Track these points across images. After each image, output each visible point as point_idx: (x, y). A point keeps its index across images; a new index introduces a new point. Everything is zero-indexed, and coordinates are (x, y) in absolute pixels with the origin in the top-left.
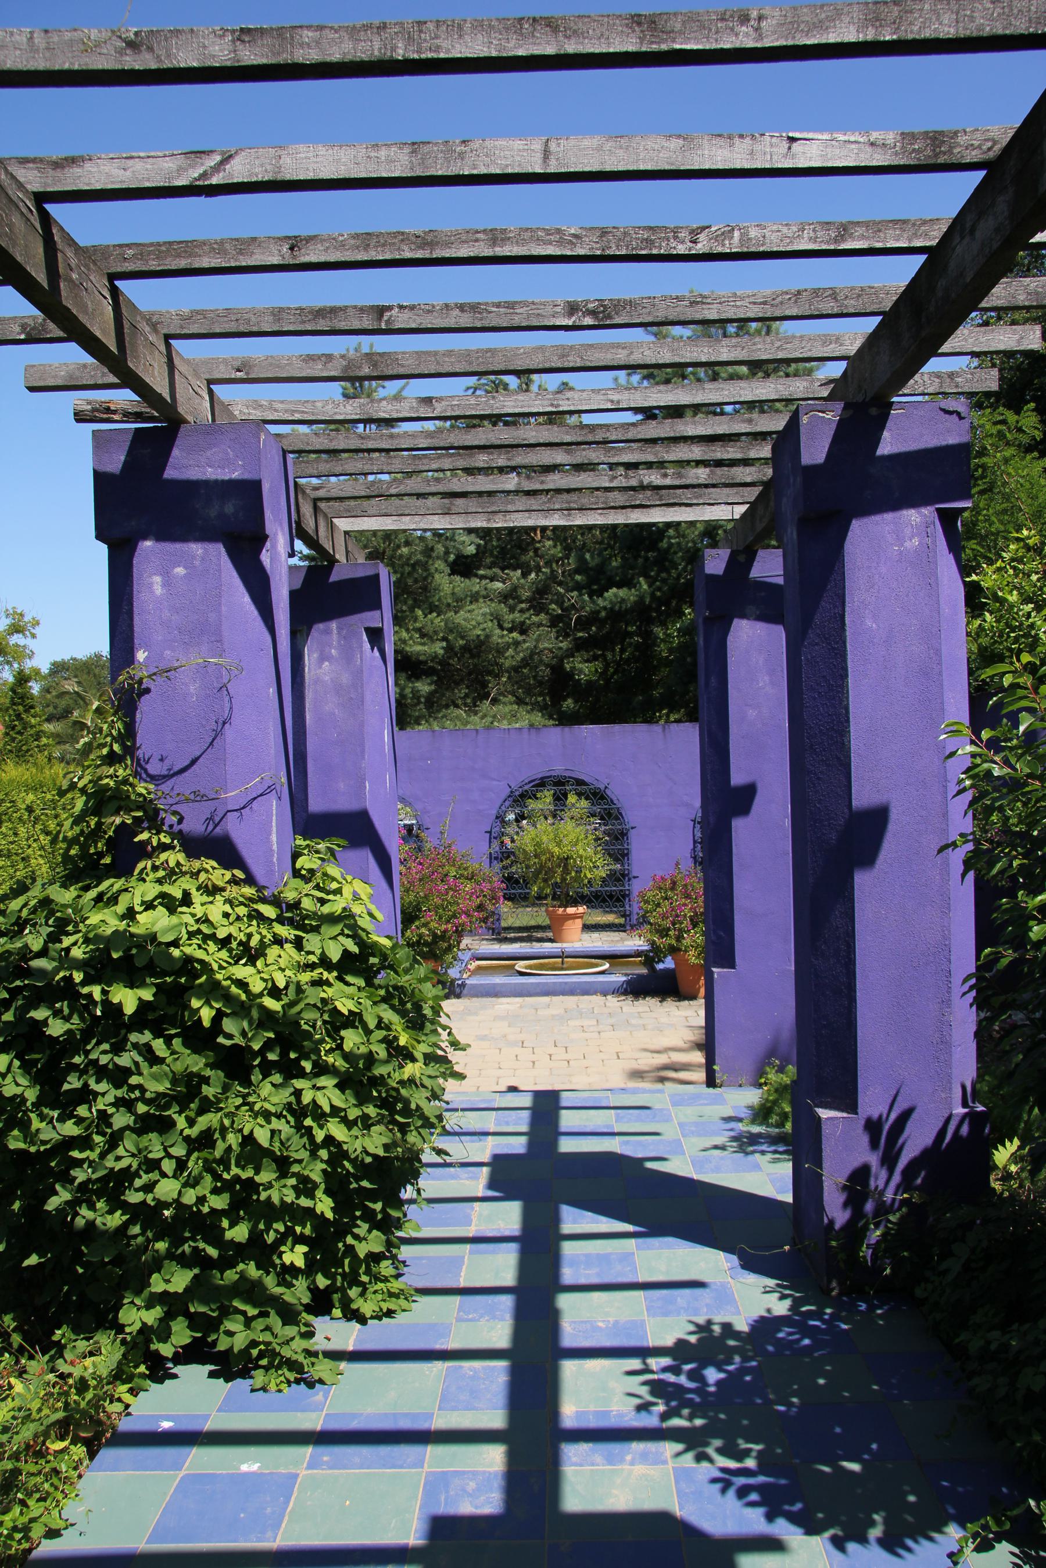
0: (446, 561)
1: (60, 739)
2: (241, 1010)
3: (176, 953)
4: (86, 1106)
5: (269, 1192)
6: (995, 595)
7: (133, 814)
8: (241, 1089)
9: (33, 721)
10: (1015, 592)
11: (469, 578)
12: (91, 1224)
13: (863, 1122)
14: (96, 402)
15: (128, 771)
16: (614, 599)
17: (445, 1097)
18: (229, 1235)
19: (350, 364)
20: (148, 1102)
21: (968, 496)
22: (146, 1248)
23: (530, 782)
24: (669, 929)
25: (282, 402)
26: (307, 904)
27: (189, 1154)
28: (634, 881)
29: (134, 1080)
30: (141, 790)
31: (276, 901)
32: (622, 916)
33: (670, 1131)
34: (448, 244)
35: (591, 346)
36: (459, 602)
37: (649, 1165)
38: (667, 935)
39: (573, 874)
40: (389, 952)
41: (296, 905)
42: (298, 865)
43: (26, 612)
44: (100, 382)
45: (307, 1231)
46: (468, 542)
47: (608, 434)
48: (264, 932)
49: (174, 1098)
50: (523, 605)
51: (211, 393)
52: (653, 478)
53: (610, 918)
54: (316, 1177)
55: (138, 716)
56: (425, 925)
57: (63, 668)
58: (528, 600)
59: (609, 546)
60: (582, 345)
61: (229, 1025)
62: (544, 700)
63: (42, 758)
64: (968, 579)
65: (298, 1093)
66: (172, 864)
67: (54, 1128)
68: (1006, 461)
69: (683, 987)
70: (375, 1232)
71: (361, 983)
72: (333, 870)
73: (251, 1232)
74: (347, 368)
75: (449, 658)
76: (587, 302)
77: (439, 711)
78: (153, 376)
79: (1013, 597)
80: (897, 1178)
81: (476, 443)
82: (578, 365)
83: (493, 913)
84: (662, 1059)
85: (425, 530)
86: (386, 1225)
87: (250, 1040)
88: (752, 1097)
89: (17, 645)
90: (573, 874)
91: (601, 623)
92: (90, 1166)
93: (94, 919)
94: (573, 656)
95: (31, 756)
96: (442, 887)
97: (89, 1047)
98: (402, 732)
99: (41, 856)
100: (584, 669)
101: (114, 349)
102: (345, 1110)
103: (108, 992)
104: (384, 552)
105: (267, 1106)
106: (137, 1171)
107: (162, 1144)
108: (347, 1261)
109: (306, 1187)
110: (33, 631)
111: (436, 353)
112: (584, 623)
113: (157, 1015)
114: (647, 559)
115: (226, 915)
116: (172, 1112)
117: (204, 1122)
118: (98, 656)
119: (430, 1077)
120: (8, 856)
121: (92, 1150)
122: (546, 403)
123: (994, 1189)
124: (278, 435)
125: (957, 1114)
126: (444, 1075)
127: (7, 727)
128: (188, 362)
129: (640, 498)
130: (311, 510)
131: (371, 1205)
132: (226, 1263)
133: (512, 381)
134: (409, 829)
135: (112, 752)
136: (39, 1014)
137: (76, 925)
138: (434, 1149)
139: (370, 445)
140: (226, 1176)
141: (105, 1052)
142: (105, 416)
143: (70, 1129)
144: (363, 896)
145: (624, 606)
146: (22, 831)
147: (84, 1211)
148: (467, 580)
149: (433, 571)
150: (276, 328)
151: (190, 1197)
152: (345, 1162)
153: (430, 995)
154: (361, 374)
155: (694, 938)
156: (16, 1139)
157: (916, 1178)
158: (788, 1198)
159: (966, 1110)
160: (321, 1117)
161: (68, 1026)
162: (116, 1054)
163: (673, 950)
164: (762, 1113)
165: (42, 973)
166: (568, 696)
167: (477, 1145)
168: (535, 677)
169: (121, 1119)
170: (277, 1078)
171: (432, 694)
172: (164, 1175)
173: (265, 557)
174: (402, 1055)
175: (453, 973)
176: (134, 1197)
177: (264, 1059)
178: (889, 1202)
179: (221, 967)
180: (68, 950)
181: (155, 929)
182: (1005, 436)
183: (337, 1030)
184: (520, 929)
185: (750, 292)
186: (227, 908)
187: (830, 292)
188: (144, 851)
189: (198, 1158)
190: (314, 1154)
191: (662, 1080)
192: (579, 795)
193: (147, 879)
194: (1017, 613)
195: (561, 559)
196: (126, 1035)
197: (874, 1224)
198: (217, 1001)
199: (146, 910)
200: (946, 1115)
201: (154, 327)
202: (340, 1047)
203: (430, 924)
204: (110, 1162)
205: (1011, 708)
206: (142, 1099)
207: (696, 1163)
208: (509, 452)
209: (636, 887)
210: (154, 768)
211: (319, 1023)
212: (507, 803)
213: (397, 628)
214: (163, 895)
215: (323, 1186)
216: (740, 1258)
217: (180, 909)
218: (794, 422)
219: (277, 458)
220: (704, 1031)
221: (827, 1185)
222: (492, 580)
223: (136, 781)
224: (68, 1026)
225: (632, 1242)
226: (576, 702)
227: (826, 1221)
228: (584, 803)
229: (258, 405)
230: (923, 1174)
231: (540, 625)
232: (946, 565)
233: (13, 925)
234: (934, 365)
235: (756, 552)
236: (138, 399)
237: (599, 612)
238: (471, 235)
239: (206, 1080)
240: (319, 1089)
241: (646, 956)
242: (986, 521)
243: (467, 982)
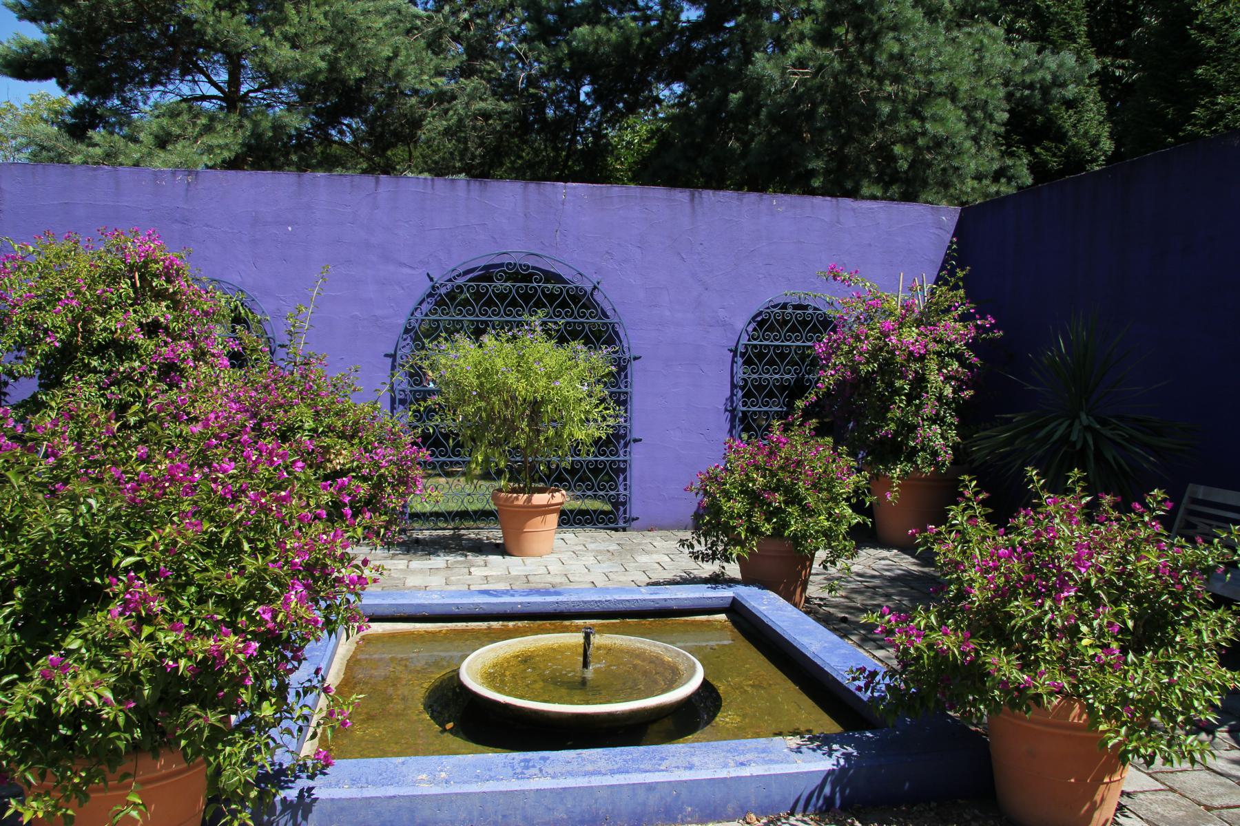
28: (634, 446)
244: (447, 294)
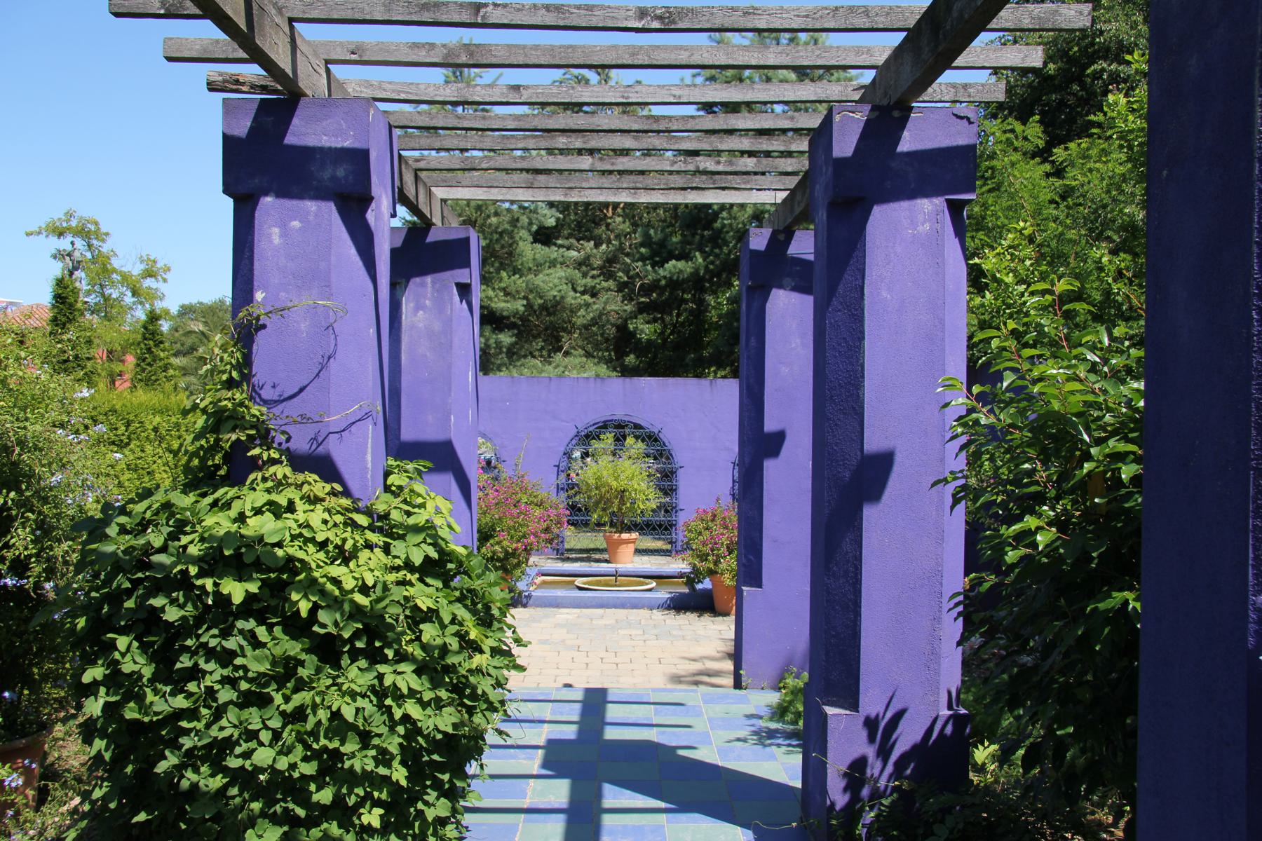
0: (529, 231)
1: (185, 372)
2: (335, 604)
3: (280, 552)
4: (195, 683)
5: (352, 761)
6: (994, 277)
7: (247, 432)
8: (332, 672)
9: (162, 355)
10: (1011, 275)
11: (549, 246)
12: (195, 786)
13: (863, 719)
14: (227, 74)
15: (244, 395)
16: (673, 270)
17: (508, 686)
18: (315, 798)
19: (451, 52)
20: (250, 681)
21: (972, 189)
22: (242, 808)
23: (594, 424)
24: (708, 555)
25: (390, 83)
26: (396, 516)
27: (284, 727)
28: (680, 513)
29: (239, 661)
30: (255, 411)
31: (368, 512)
32: (670, 543)
33: (700, 725)
35: (658, 47)
36: (538, 267)
37: (681, 752)
38: (706, 560)
39: (628, 505)
40: (464, 559)
41: (386, 516)
42: (389, 482)
43: (159, 259)
44: (230, 56)
45: (384, 796)
46: (549, 216)
47: (670, 124)
48: (357, 537)
49: (272, 677)
50: (595, 272)
51: (328, 71)
52: (708, 164)
53: (659, 544)
54: (394, 749)
55: (255, 347)
56: (499, 543)
57: (191, 310)
58: (601, 268)
59: (671, 225)
60: (650, 46)
61: (323, 616)
62: (610, 355)
63: (168, 387)
64: (971, 262)
65: (380, 677)
66: (280, 476)
67: (166, 701)
68: (1013, 164)
69: (718, 605)
70: (442, 799)
71: (439, 584)
72: (419, 487)
73: (335, 796)
74: (447, 56)
75: (529, 315)
76: (655, 8)
77: (518, 360)
78: (278, 53)
79: (1009, 279)
80: (890, 768)
81: (557, 127)
82: (646, 63)
83: (558, 536)
84: (697, 666)
85: (512, 202)
86: (453, 794)
87: (341, 629)
88: (774, 698)
89: (150, 288)
90: (628, 505)
91: (663, 289)
92: (196, 735)
93: (209, 521)
94: (636, 318)
95: (160, 384)
96: (515, 512)
97: (200, 632)
98: (486, 377)
99: (165, 471)
100: (645, 329)
101: (243, 27)
102: (420, 692)
103: (219, 584)
104: (476, 221)
105: (353, 686)
106: (238, 740)
107: (261, 717)
108: (417, 824)
109: (384, 758)
110: (164, 276)
111: (524, 47)
112: (646, 290)
113: (261, 605)
114: (702, 236)
115: (325, 522)
116: (270, 689)
117: (298, 699)
118: (222, 302)
119: (495, 667)
120: (136, 470)
121: (199, 721)
122: (618, 94)
123: (972, 781)
124: (385, 112)
125: (943, 716)
126: (507, 667)
127: (138, 359)
128: (309, 43)
129: (697, 181)
130: (413, 179)
131: (439, 775)
132: (311, 822)
133: (590, 75)
134: (489, 462)
135: (231, 379)
136: (158, 602)
137: (194, 526)
138: (497, 730)
139: (466, 124)
140: (315, 746)
141: (214, 636)
142: (234, 87)
143: (180, 702)
144: (444, 511)
145: (681, 277)
146: (149, 448)
147: (189, 774)
148: (547, 249)
149: (517, 239)
150: (386, 18)
151: (283, 764)
152: (419, 738)
153: (498, 598)
154: (459, 61)
155: (729, 563)
156: (132, 710)
157: (907, 769)
158: (798, 784)
159: (951, 712)
160: (399, 697)
161: (182, 613)
162: (224, 639)
163: (711, 573)
164: (780, 712)
165: (161, 566)
166: (630, 352)
167: (535, 731)
168: (602, 335)
169: (225, 695)
170: (363, 663)
171: (513, 345)
172: (261, 744)
173: (370, 216)
174: (472, 648)
175: (521, 586)
176: (233, 763)
177: (353, 646)
178: (882, 788)
179: (319, 566)
180: (185, 547)
181: (262, 531)
182: (1012, 144)
183: (417, 624)
184: (581, 551)
185: (794, 6)
186: (326, 516)
187: (864, 9)
188: (255, 464)
189: (292, 730)
190: (392, 729)
191: (697, 683)
192: (637, 437)
193: (258, 488)
194: (1011, 293)
195: (629, 233)
196: (233, 622)
197: (869, 807)
198: (314, 595)
199: (255, 515)
200: (934, 716)
201: (280, 10)
202: (418, 639)
203: (503, 543)
204: (214, 732)
205: (997, 368)
206: (245, 678)
207: (722, 752)
208: (584, 136)
209: (681, 518)
210: (267, 394)
211: (402, 617)
212: (574, 442)
213: (484, 287)
214: (271, 503)
215: (399, 758)
216: (755, 833)
217: (284, 515)
218: (828, 121)
219: (383, 131)
220: (733, 643)
221: (831, 773)
222: (568, 249)
223: (251, 404)
224: (182, 613)
225: (664, 816)
226: (637, 357)
227: (828, 802)
228: (640, 445)
229: (368, 84)
230: (912, 766)
231: (609, 289)
232: (952, 245)
233: (137, 525)
234: (948, 76)
235: (794, 232)
236: (265, 74)
237: (660, 280)
239: (302, 663)
240: (399, 673)
241: (688, 577)
242: (993, 215)
243: (533, 594)
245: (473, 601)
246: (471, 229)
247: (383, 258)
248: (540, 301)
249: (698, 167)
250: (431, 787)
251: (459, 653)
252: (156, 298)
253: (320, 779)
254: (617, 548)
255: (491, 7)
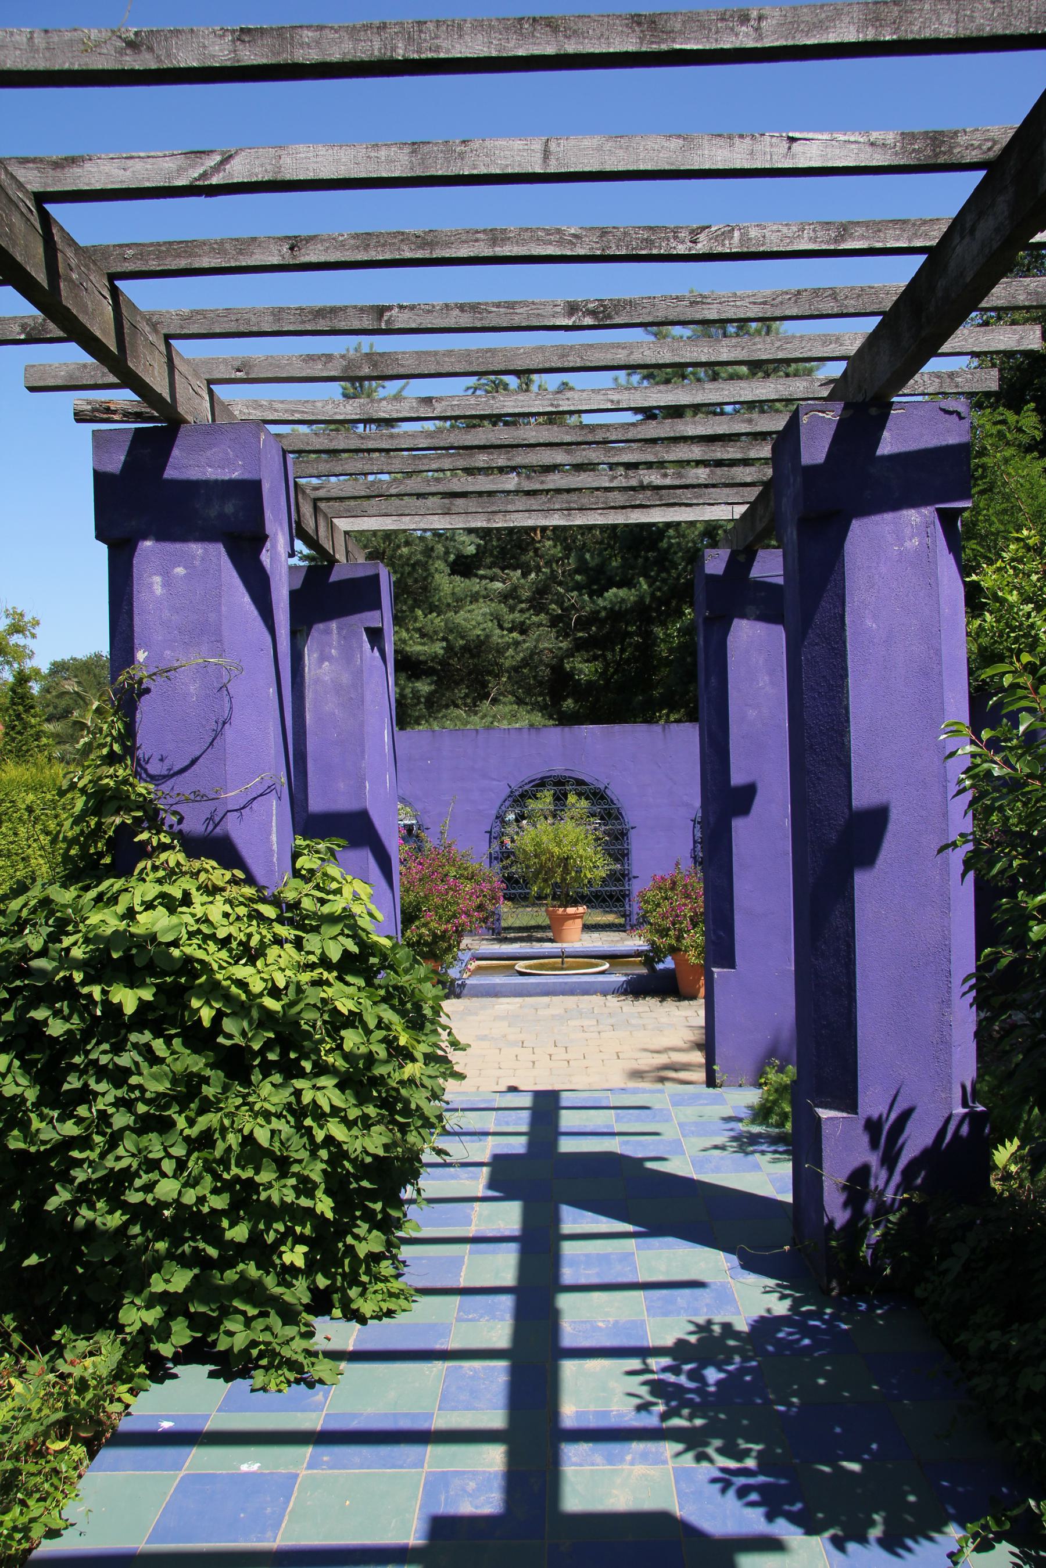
0: (446, 561)
1: (59, 739)
2: (241, 1010)
3: (176, 953)
4: (86, 1106)
5: (269, 1192)
6: (995, 595)
7: (133, 814)
8: (241, 1089)
9: (33, 721)
10: (1015, 592)
11: (469, 578)
12: (91, 1224)
13: (863, 1122)
15: (128, 771)
16: (614, 599)
17: (445, 1097)
18: (229, 1235)
19: (351, 364)
20: (148, 1102)
21: (968, 496)
22: (146, 1248)
23: (530, 782)
24: (669, 929)
25: (282, 402)
26: (307, 904)
27: (189, 1154)
28: (634, 881)
29: (134, 1080)
30: (141, 790)
31: (276, 901)
32: (622, 916)
33: (670, 1131)
34: (448, 244)
35: (591, 346)
36: (459, 602)
37: (649, 1165)
38: (667, 935)
39: (573, 874)
40: (389, 952)
41: (296, 905)
42: (298, 866)
43: (26, 612)
44: (100, 382)
45: (307, 1231)
46: (468, 542)
47: (608, 434)
48: (264, 932)
49: (174, 1098)
50: (523, 605)
51: (211, 393)
52: (653, 478)
53: (610, 918)
54: (316, 1177)
55: (138, 716)
56: (425, 925)
57: (63, 668)
58: (528, 600)
60: (582, 345)
61: (229, 1025)
62: (544, 700)
63: (42, 758)
64: (968, 579)
65: (298, 1093)
66: (172, 864)
67: (54, 1128)
68: (1006, 461)
69: (683, 986)
70: (375, 1232)
71: (361, 983)
72: (333, 870)
73: (251, 1232)
74: (347, 368)
75: (449, 658)
76: (587, 302)
77: (439, 711)
79: (1013, 597)
80: (897, 1178)
81: (476, 443)
82: (578, 365)
83: (493, 913)
84: (662, 1059)
85: (425, 530)
86: (386, 1225)
87: (250, 1040)
88: (752, 1097)
89: (17, 645)
90: (573, 874)
91: (601, 622)
92: (90, 1166)
93: (94, 919)
94: (573, 656)
95: (31, 756)
96: (442, 887)
97: (89, 1047)
98: (402, 732)
99: (41, 856)
100: (584, 669)
101: (114, 349)
102: (345, 1110)
103: (109, 992)
104: (384, 552)
105: (267, 1106)
106: (137, 1171)
107: (162, 1144)
108: (347, 1261)
109: (306, 1187)
110: (33, 631)
111: (436, 353)
112: (583, 623)
113: (156, 1015)
114: (647, 559)
115: (226, 915)
116: (172, 1112)
117: (204, 1122)
118: (98, 656)
119: (430, 1077)
120: (8, 856)
121: (92, 1150)
122: (546, 403)
123: (994, 1189)
124: (278, 435)
125: (957, 1115)
126: (444, 1075)
127: (7, 727)
128: (188, 362)
129: (640, 498)
130: (311, 510)
131: (371, 1205)
132: (226, 1263)
133: (512, 381)
134: (409, 829)
135: (112, 752)
136: (39, 1014)
137: (76, 925)
138: (434, 1149)
139: (371, 445)
140: (226, 1176)
141: (105, 1052)
142: (105, 416)
143: (70, 1129)
144: (363, 897)
145: (624, 606)
146: (22, 830)
147: (84, 1211)
148: (467, 581)
149: (433, 571)
150: (275, 328)
151: (190, 1197)
152: (345, 1162)
153: (430, 996)
154: (361, 374)
155: (694, 938)
156: (16, 1139)
157: (916, 1178)
158: (788, 1198)
159: (966, 1110)
160: (321, 1117)
161: (68, 1026)
162: (116, 1054)
163: (673, 950)
164: (762, 1113)
165: (42, 973)
166: (567, 696)
168: (535, 677)
169: (121, 1119)
170: (277, 1078)
171: (432, 694)
172: (164, 1175)
173: (265, 557)
174: (402, 1055)
175: (453, 973)
176: (134, 1197)
177: (264, 1059)
178: (889, 1201)
179: (221, 967)
180: (68, 950)
181: (155, 929)
182: (1005, 436)
183: (337, 1030)
184: (520, 929)
186: (227, 908)
187: (830, 292)
188: (144, 851)
189: (198, 1158)
190: (314, 1154)
191: (662, 1080)
192: (579, 795)
193: (147, 879)
194: (1017, 613)
195: (561, 559)
196: (126, 1035)
197: (875, 1224)
198: (217, 1001)
199: (146, 910)
200: (946, 1115)
201: (154, 327)
202: (340, 1047)
203: (431, 924)
204: (110, 1162)
205: (1011, 708)
206: (142, 1099)
207: (696, 1163)
208: (509, 452)
209: (636, 887)
210: (154, 768)
211: (319, 1023)
212: (507, 803)
213: (397, 628)
214: (163, 895)
215: (323, 1186)
216: (740, 1258)
217: (180, 909)
218: (794, 422)
219: (276, 458)
220: (703, 1031)
221: (827, 1184)
222: (492, 580)
223: (136, 781)
224: (68, 1026)
225: (632, 1242)
226: (576, 702)
227: (826, 1221)
228: (584, 803)
229: (258, 405)
230: (923, 1174)
231: (540, 625)
232: (946, 565)
233: (13, 925)
234: (934, 365)
235: (756, 551)
236: (138, 399)
237: (599, 612)
238: (471, 235)
239: (206, 1080)
240: (319, 1089)
241: (646, 956)
242: (986, 520)
243: (467, 982)
244: (520, 796)
245: (401, 1000)
246: (381, 565)
247: (282, 605)
248: (462, 642)
249: (641, 482)
250: (362, 1218)
251: (387, 1062)
252: (24, 657)
253: (233, 1214)
254: (563, 925)
255: (397, 310)
